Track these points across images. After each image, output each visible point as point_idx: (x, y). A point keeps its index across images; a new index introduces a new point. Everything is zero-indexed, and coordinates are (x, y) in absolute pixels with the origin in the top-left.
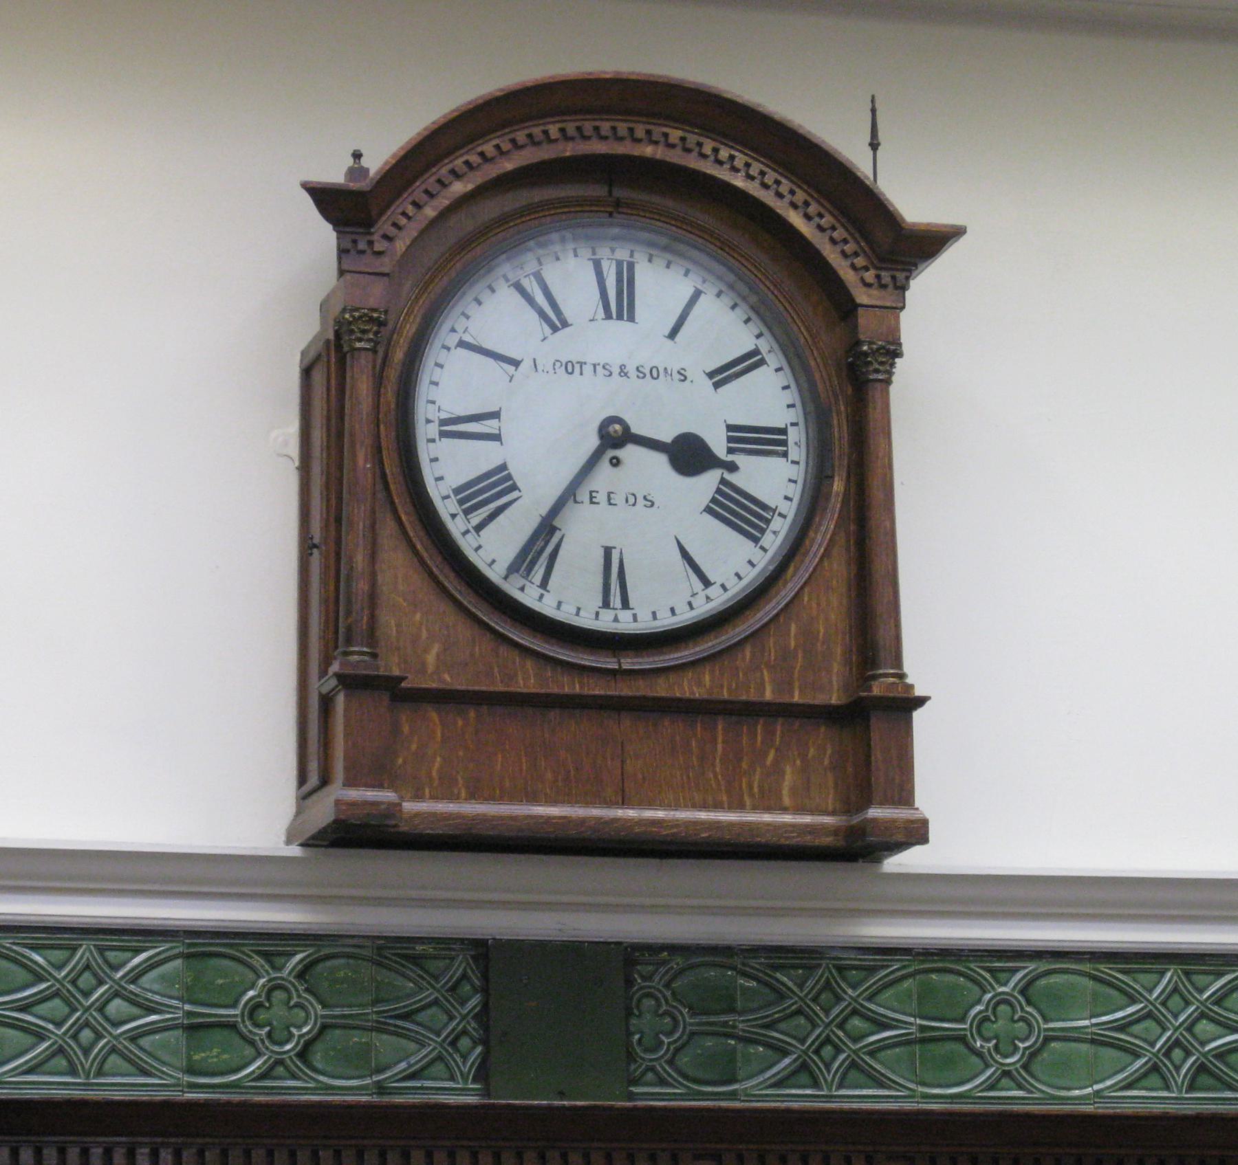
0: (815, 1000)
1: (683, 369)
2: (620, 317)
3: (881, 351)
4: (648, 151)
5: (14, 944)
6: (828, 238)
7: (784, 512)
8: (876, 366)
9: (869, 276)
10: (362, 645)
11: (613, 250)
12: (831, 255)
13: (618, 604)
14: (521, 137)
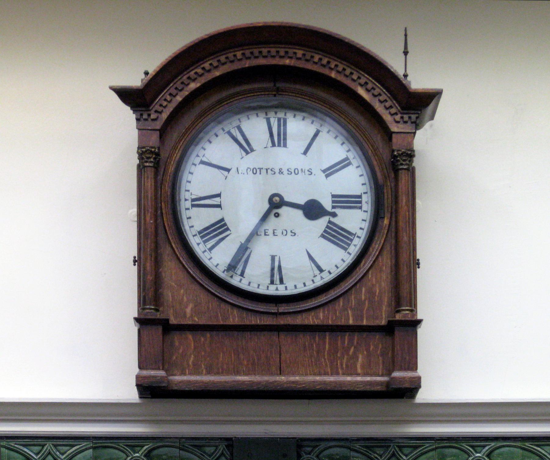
1: (310, 169)
2: (279, 145)
3: (404, 154)
4: (287, 62)
5: (16, 444)
6: (377, 100)
7: (360, 235)
8: (402, 162)
9: (398, 118)
10: (151, 305)
11: (276, 113)
12: (379, 108)
13: (278, 282)
14: (223, 59)
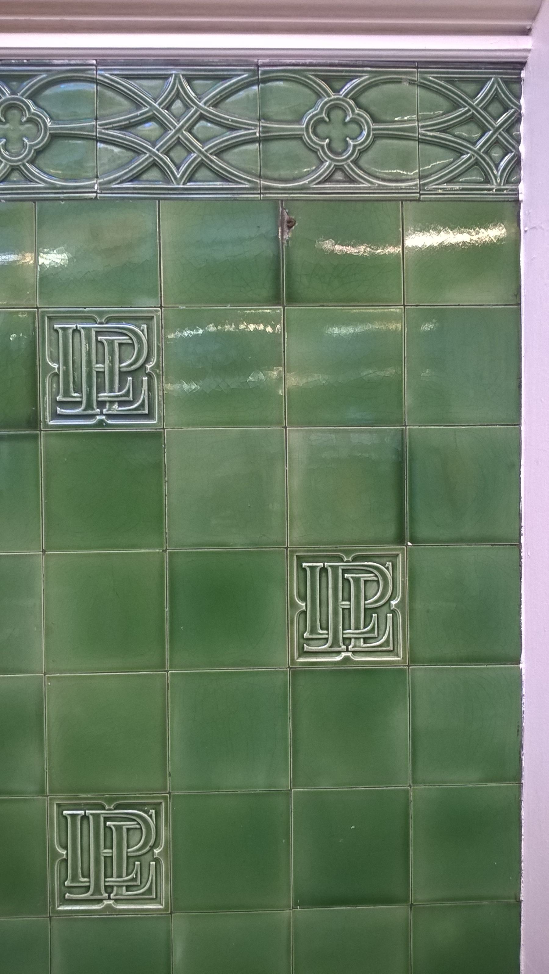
0: (485, 108)
